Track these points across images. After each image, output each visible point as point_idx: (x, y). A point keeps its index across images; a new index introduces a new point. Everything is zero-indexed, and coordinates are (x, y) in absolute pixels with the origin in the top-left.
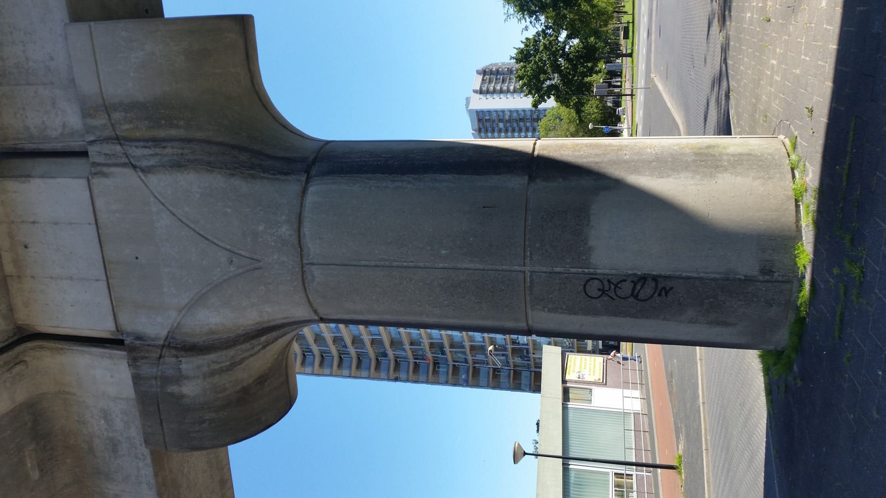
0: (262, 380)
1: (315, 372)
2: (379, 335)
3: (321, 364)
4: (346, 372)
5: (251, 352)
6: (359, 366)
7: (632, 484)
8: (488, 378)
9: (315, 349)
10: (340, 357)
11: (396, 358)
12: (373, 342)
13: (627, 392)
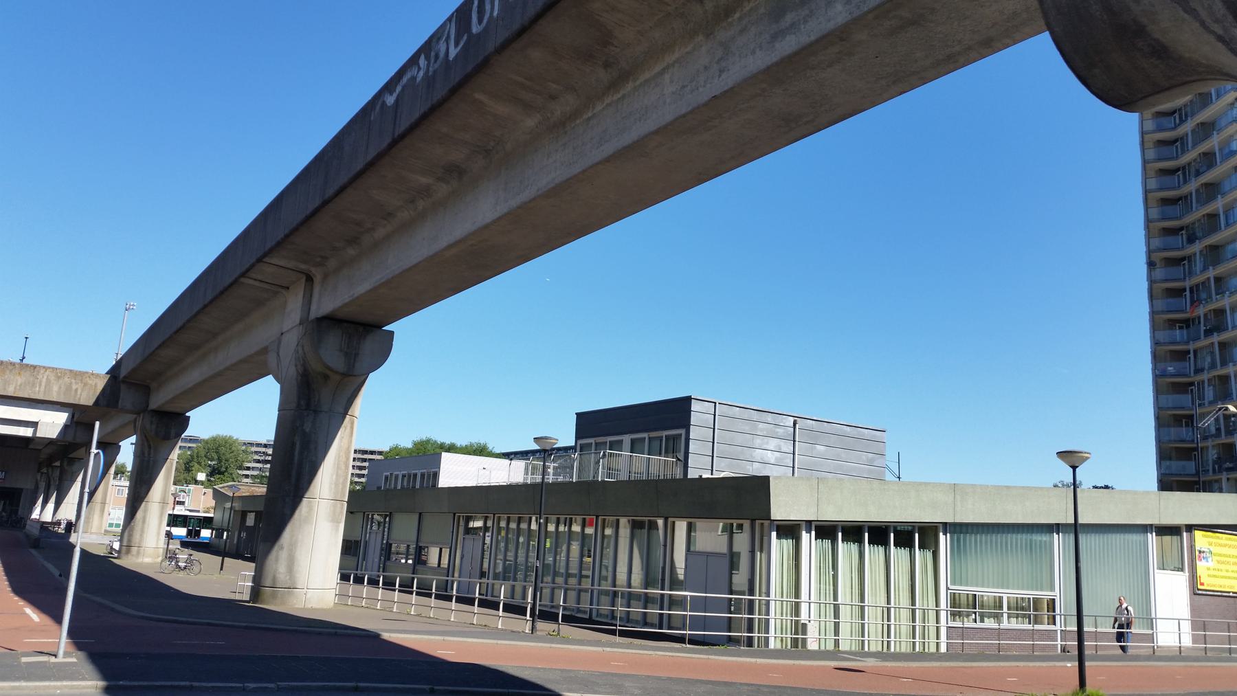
0: (1161, 52)
1: (1146, 137)
2: (1228, 225)
3: (1161, 143)
4: (1153, 184)
5: (1208, 21)
6: (1165, 202)
7: (1042, 623)
8: (1174, 408)
9: (1188, 127)
10: (1178, 170)
11: (1189, 258)
12: (1213, 216)
13: (1186, 627)
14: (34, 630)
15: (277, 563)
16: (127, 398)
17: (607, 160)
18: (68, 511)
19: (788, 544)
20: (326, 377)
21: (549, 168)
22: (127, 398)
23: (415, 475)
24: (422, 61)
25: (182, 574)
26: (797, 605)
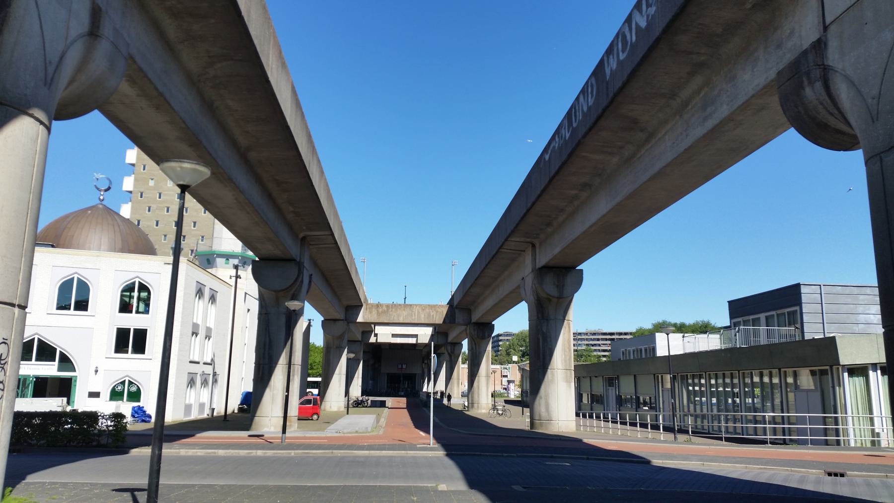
14: (422, 438)
15: (540, 405)
16: (460, 317)
17: (649, 180)
18: (441, 386)
19: (859, 381)
20: (550, 300)
21: (626, 185)
22: (460, 317)
23: (641, 350)
24: (557, 139)
25: (501, 418)
26: (872, 420)
